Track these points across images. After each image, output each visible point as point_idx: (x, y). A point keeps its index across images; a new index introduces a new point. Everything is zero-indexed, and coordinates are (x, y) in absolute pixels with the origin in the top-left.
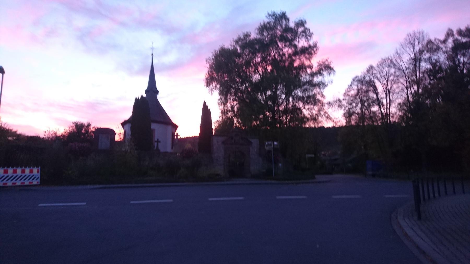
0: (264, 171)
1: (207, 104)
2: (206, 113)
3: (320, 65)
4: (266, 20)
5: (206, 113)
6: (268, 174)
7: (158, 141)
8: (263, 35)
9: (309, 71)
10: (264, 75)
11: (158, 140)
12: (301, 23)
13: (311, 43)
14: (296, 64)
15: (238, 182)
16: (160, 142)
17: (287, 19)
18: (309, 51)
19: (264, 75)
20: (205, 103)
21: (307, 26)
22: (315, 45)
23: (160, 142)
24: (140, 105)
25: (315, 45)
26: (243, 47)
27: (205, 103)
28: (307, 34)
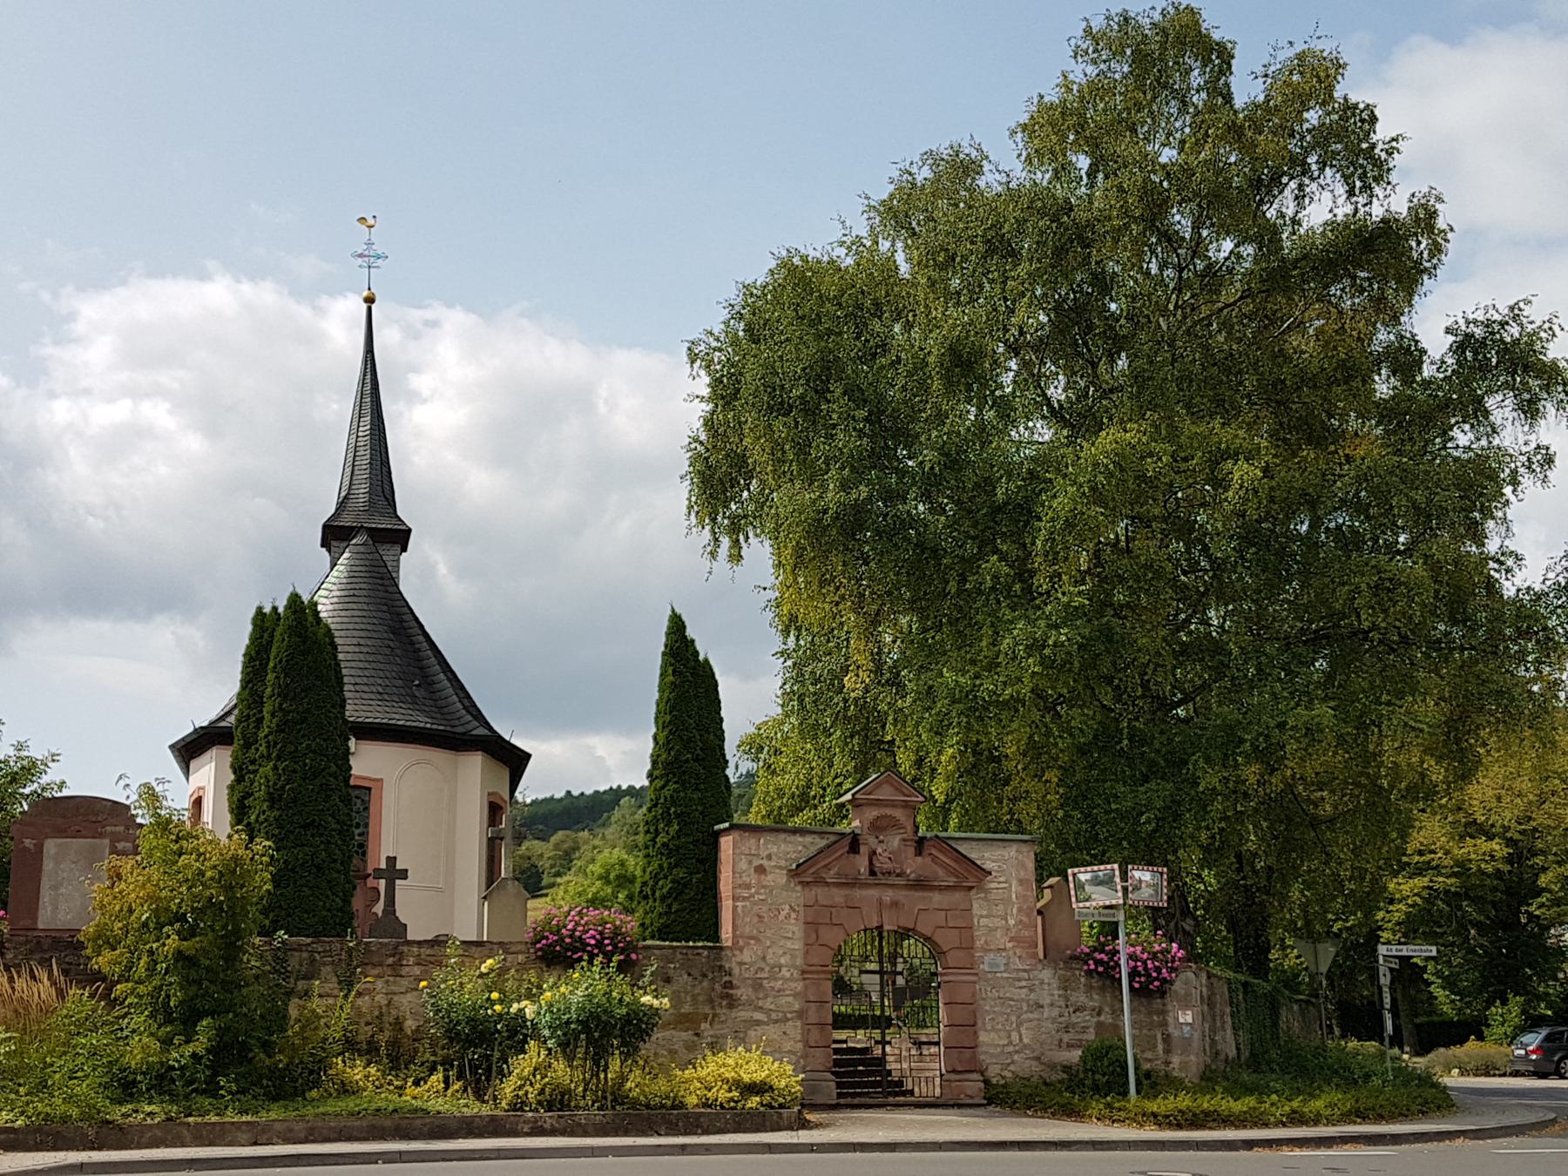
0: (1075, 1055)
1: (690, 632)
2: (688, 685)
3: (1464, 344)
4: (1082, 72)
5: (688, 685)
6: (1090, 1082)
7: (394, 873)
8: (1063, 170)
9: (1384, 386)
10: (741, 538)
11: (392, 861)
12: (1314, 76)
13: (1392, 202)
14: (1304, 345)
15: (880, 1136)
16: (404, 874)
17: (1219, 57)
18: (1392, 255)
19: (741, 538)
20: (677, 626)
21: (1352, 89)
22: (1424, 217)
23: (404, 874)
24: (286, 648)
25: (1424, 217)
26: (940, 260)
27: (677, 626)
28: (1355, 148)
